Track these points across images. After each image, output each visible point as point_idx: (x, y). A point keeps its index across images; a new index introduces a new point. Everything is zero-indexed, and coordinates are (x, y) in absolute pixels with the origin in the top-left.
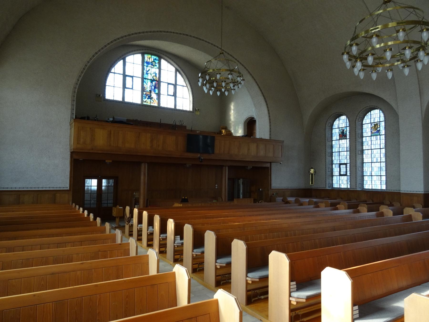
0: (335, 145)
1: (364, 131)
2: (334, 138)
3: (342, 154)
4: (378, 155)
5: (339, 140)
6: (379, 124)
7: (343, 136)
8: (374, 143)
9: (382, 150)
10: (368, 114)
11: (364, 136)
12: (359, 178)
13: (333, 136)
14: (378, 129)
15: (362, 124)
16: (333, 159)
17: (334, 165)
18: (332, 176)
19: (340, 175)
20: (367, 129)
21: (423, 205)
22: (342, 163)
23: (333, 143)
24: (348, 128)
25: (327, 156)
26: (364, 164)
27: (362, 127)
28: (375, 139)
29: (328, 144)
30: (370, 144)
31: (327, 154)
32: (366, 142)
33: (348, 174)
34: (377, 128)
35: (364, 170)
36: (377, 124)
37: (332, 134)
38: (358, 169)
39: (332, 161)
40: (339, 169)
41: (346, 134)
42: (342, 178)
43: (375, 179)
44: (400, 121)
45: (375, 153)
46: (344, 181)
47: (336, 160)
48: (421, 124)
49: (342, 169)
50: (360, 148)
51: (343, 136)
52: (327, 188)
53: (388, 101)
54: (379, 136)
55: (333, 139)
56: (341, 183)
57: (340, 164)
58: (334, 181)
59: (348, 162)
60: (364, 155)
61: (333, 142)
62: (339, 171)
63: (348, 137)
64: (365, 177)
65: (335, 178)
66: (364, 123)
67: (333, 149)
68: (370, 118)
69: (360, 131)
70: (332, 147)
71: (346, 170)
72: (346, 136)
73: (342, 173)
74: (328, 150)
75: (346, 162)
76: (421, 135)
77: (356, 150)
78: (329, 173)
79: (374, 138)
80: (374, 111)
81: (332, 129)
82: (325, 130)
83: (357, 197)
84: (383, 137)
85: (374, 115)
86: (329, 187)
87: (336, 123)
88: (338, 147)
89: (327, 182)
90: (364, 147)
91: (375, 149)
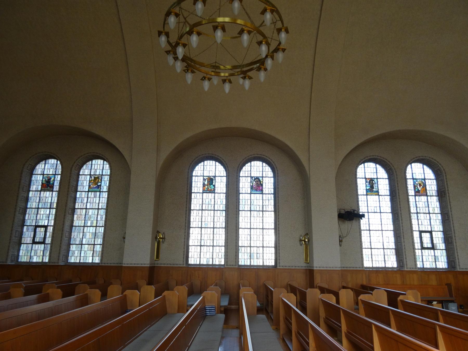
0: (32, 199)
1: (79, 184)
2: (33, 188)
3: (42, 211)
4: (94, 218)
5: (41, 191)
6: (100, 178)
7: (47, 185)
8: (92, 202)
9: (100, 211)
10: (88, 163)
11: (79, 189)
12: (64, 247)
13: (32, 184)
14: (99, 184)
15: (79, 175)
16: (26, 218)
17: (25, 227)
18: (20, 244)
19: (34, 242)
20: (84, 182)
21: (147, 280)
22: (40, 224)
23: (30, 195)
24: (59, 178)
25: (17, 213)
26: (74, 228)
27: (78, 177)
28: (93, 196)
29: (22, 194)
30: (85, 201)
31: (18, 209)
32: (80, 199)
33: (48, 240)
34: (98, 182)
35: (72, 237)
36: (98, 178)
37: (30, 181)
38: (64, 235)
39: (24, 221)
40: (33, 233)
41: (53, 184)
42: (36, 247)
43: (86, 249)
44: (133, 177)
45: (90, 213)
46: (39, 252)
47: (30, 219)
48: (155, 184)
49: (38, 233)
50: (24, 205)
51: (47, 185)
52: (9, 263)
53: (121, 150)
54: (98, 193)
55: (31, 189)
56: (32, 254)
57: (36, 226)
58: (21, 251)
59: (52, 223)
60: (75, 216)
61: (31, 193)
62: (32, 236)
63: (56, 188)
64: (71, 246)
65: (23, 247)
66: (81, 173)
67: (29, 204)
68: (90, 168)
69: (75, 183)
70: (27, 199)
71: (45, 235)
72: (52, 187)
73: (37, 240)
74: (21, 204)
75: (46, 224)
76: (153, 196)
77: (66, 208)
78: (15, 239)
79: (91, 195)
80: (255, 162)
81: (32, 174)
82: (21, 173)
83: (62, 276)
84: (105, 195)
85: (96, 166)
86: (12, 261)
87: (40, 168)
88: (38, 201)
89: (10, 253)
90: (77, 204)
91: (92, 209)
